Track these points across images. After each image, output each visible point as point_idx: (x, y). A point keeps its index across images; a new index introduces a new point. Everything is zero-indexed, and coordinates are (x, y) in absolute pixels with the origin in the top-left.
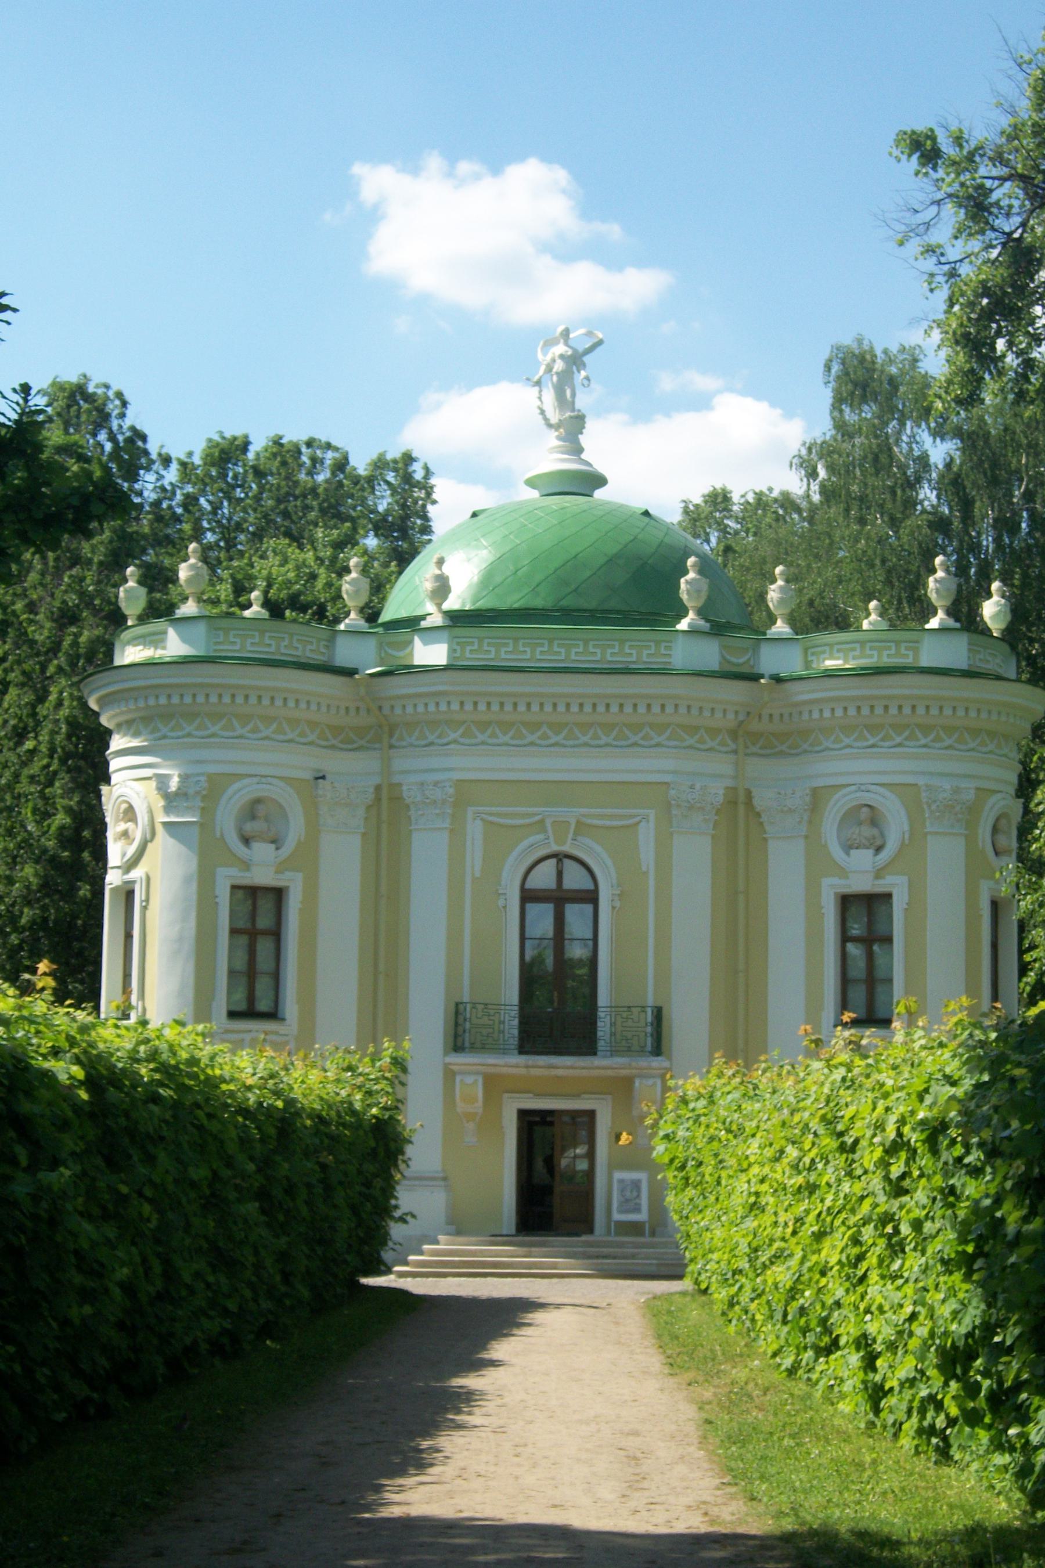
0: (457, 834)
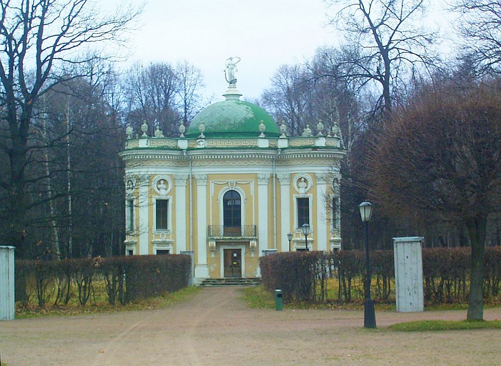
0: (208, 186)
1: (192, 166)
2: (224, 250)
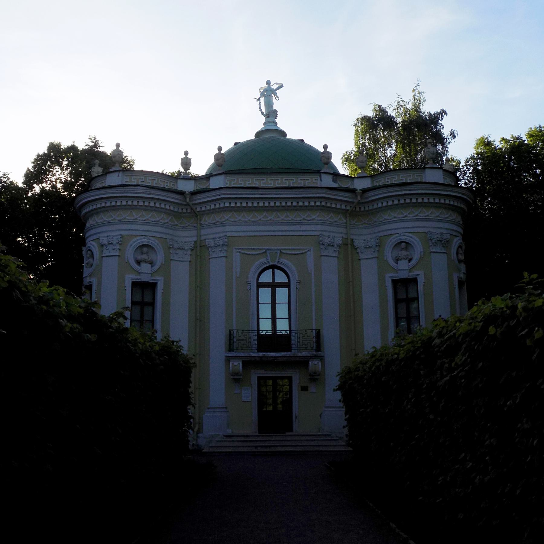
1: (201, 224)
2: (259, 378)
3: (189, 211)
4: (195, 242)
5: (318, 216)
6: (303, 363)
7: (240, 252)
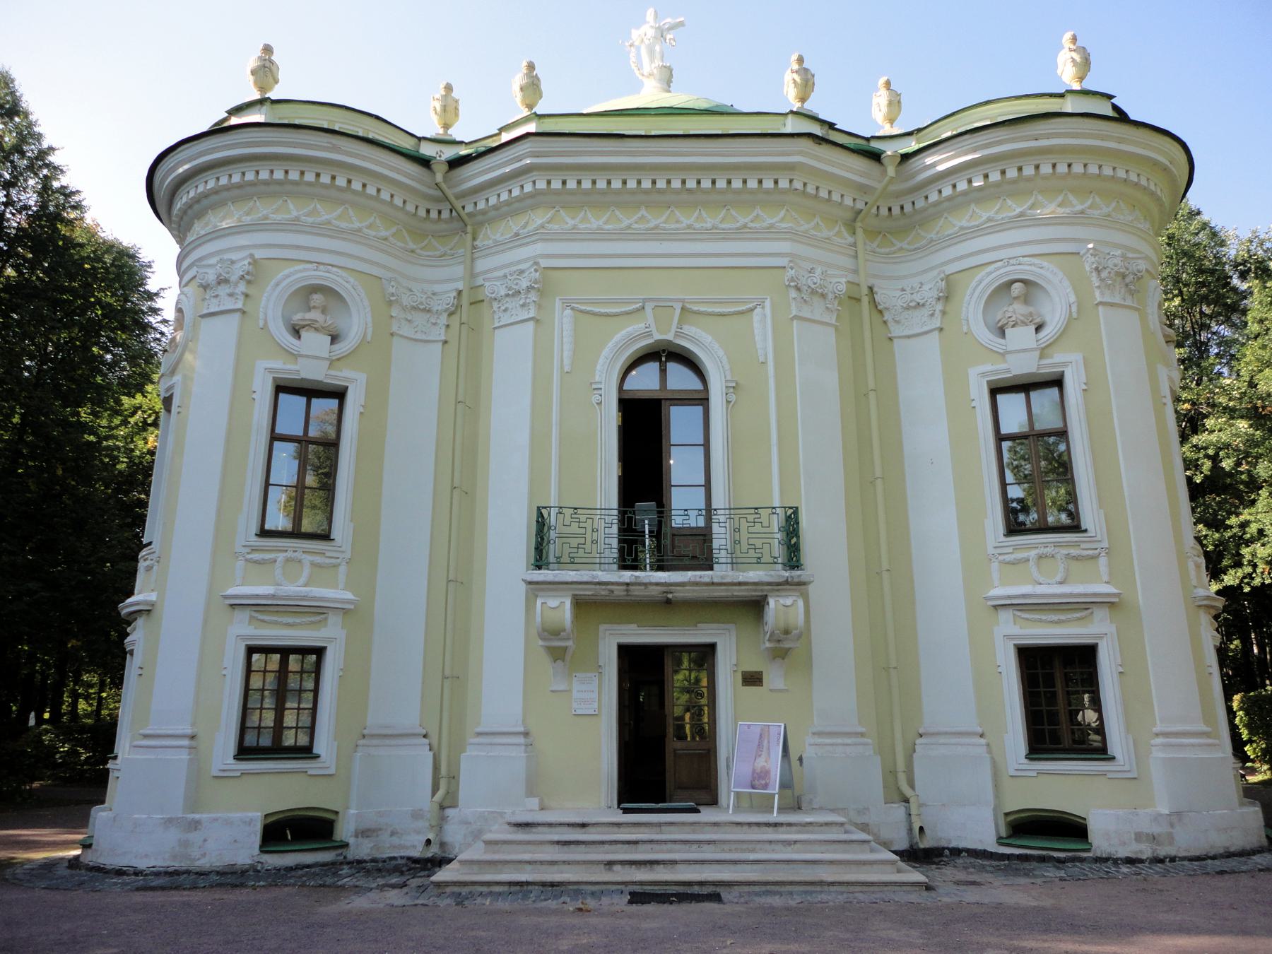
1: (474, 247)
3: (445, 214)
4: (460, 292)
5: (782, 220)
6: (752, 606)
7: (573, 309)
